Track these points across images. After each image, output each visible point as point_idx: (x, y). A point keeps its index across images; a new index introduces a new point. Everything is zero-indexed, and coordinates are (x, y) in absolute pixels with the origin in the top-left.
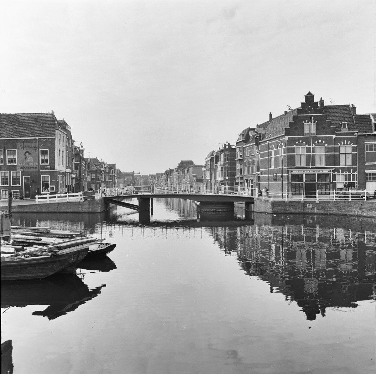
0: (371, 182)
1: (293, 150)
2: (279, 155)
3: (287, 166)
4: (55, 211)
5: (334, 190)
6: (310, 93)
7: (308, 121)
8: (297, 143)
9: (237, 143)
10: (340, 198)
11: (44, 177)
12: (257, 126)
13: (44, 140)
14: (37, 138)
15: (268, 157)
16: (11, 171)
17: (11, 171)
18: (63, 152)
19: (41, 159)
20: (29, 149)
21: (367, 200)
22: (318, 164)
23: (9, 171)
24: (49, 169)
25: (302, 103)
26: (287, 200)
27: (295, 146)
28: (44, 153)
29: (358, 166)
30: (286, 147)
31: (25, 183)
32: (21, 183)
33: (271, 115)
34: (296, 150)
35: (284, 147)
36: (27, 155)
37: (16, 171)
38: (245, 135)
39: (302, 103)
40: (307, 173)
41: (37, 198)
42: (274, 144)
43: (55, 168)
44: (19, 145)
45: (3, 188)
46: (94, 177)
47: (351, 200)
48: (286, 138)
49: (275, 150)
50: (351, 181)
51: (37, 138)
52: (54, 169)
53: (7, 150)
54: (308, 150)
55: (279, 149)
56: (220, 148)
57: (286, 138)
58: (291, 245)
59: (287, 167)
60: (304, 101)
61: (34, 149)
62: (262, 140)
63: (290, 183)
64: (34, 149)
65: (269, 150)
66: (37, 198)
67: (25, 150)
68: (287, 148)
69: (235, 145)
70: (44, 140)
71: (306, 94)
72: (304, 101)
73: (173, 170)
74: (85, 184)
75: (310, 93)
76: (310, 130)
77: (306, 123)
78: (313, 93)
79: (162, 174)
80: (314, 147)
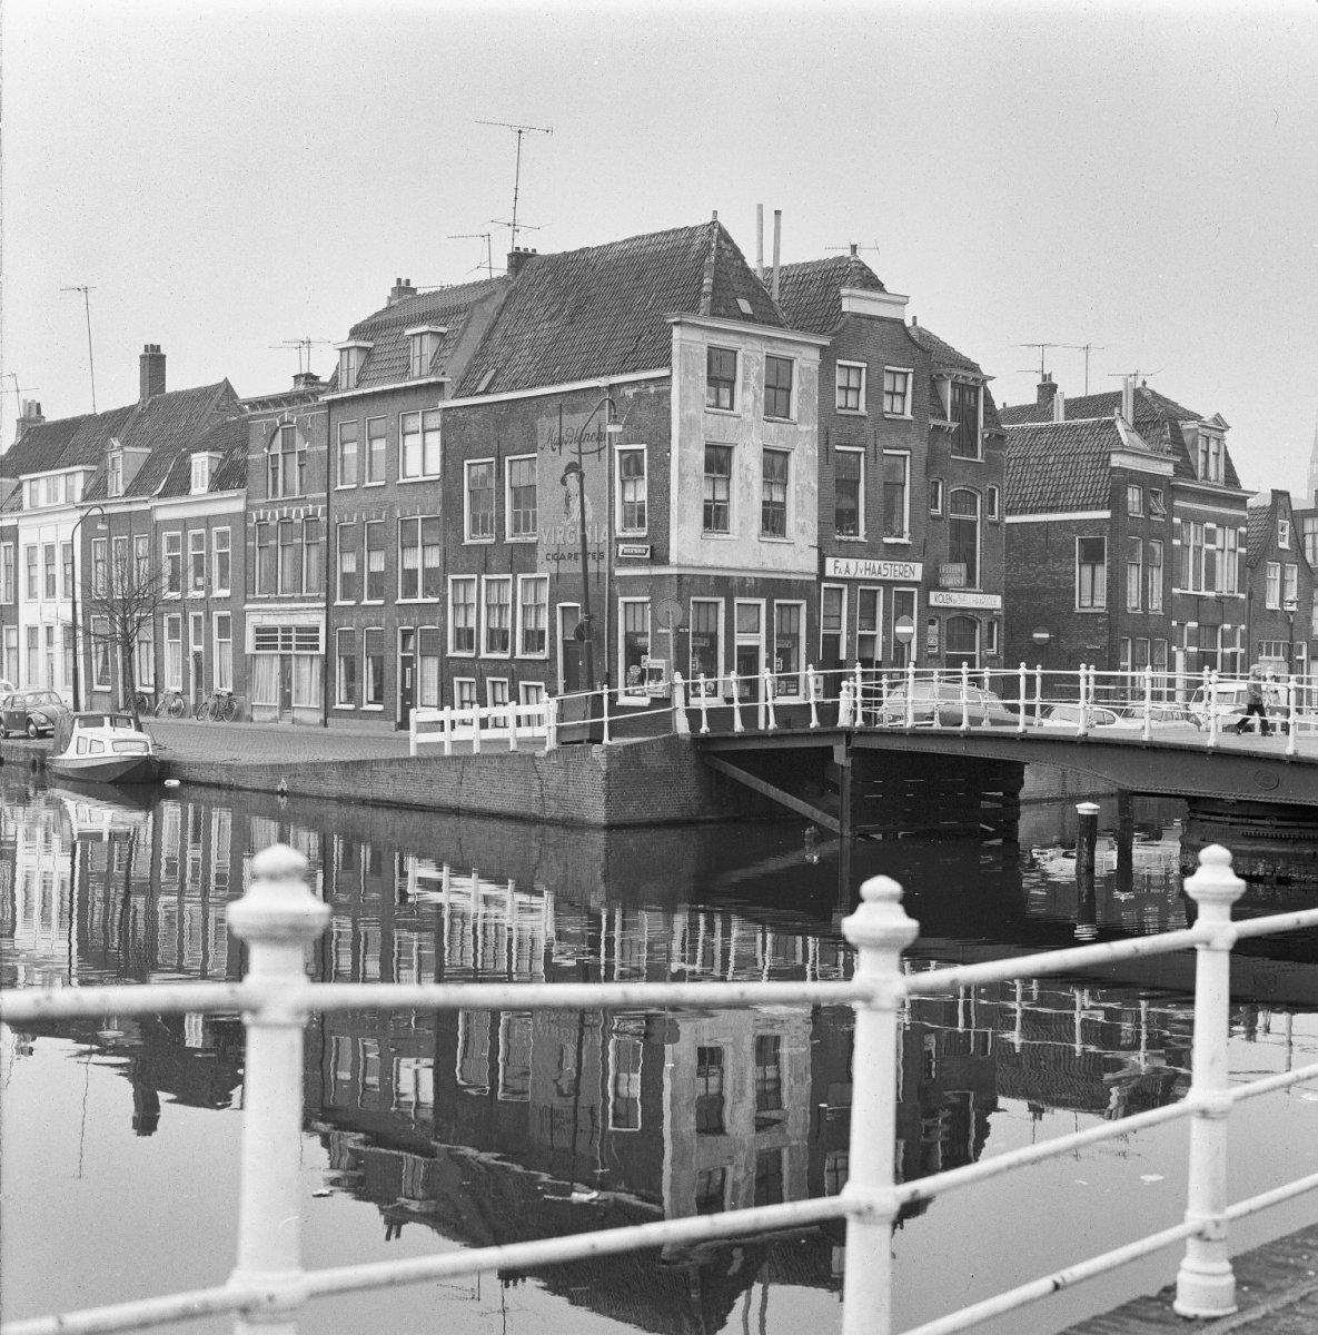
0: (738, 565)
4: (451, 801)
5: (606, 686)
10: (213, 877)
11: (630, 607)
13: (630, 392)
14: (602, 382)
16: (520, 576)
19: (623, 502)
24: (638, 562)
28: (632, 466)
29: (1056, 429)
31: (565, 642)
32: (550, 647)
37: (534, 576)
41: (1031, 672)
43: (673, 558)
44: (546, 425)
45: (491, 667)
46: (1294, 608)
50: (1200, 590)
51: (602, 382)
52: (665, 561)
53: (507, 458)
58: (523, 1201)
66: (1031, 672)
70: (630, 392)
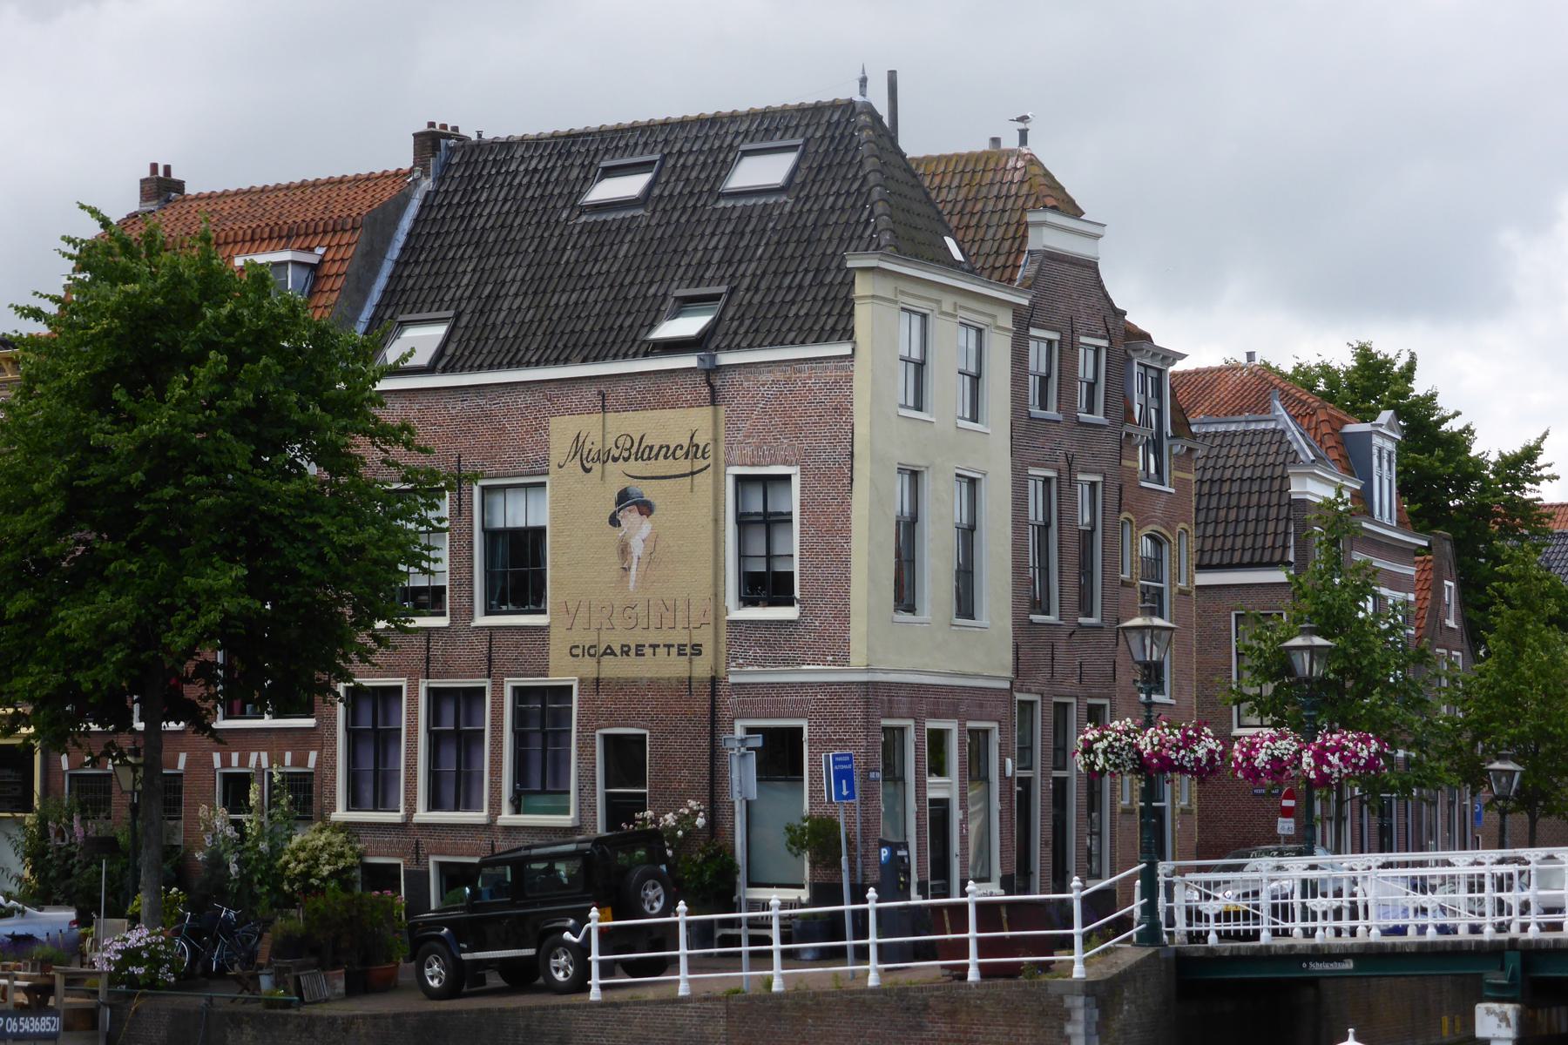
17: (509, 684)
20: (636, 467)
36: (630, 518)
47: (985, 971)
61: (684, 466)
64: (684, 466)
67: (617, 477)
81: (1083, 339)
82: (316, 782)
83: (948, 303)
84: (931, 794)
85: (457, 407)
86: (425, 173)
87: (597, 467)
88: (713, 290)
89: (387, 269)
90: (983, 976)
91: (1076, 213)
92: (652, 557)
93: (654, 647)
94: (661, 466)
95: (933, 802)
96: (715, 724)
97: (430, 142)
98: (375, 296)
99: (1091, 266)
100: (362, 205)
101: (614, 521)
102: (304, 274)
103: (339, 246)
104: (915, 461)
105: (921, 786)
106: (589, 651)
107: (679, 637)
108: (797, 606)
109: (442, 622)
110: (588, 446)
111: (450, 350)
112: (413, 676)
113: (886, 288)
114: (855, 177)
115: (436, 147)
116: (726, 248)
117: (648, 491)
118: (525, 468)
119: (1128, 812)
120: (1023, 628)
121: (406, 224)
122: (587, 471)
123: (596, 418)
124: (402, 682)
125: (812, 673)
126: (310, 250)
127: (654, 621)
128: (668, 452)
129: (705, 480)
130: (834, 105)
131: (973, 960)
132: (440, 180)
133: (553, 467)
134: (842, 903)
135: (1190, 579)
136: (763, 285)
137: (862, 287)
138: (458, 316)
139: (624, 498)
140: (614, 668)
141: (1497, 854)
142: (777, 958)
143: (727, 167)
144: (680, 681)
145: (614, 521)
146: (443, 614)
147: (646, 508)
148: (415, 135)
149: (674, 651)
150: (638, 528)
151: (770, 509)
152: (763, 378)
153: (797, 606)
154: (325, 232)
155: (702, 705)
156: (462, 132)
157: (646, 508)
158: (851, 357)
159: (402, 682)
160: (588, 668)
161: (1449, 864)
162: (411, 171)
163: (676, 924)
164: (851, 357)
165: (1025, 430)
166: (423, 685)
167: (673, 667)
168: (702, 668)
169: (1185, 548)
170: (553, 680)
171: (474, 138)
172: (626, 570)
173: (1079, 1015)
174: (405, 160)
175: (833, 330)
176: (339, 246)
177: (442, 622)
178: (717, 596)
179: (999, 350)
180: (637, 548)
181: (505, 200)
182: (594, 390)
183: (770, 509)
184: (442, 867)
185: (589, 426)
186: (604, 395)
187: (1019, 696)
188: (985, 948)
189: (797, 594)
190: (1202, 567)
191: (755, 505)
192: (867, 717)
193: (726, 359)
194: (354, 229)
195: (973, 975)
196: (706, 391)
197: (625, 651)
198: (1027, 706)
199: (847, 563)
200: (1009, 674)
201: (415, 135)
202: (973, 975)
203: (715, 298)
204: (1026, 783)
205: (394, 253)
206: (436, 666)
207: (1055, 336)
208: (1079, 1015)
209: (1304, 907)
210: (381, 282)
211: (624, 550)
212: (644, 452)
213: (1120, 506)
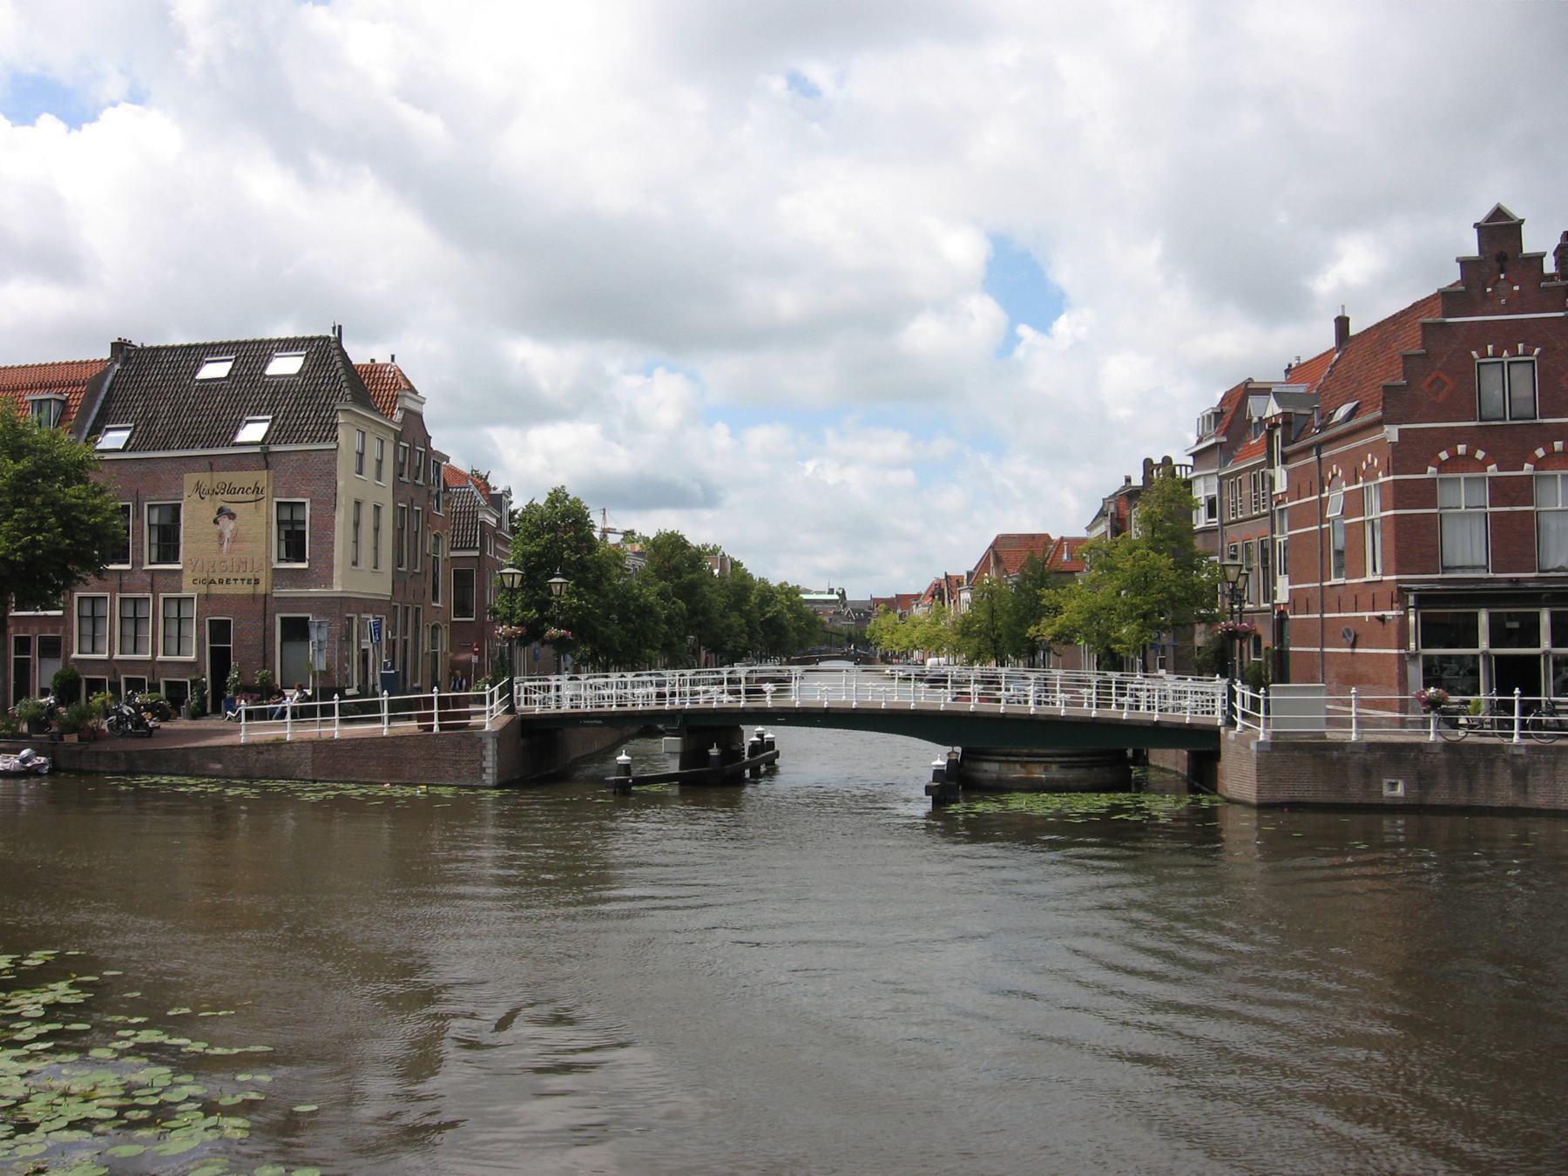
1: (1426, 493)
2: (1361, 519)
3: (1397, 573)
6: (1499, 213)
7: (1494, 351)
8: (1444, 456)
9: (1195, 455)
12: (1287, 371)
15: (1317, 528)
17: (162, 595)
18: (377, 508)
20: (227, 497)
21: (1522, 736)
22: (1232, 571)
23: (151, 596)
25: (1465, 263)
26: (1354, 737)
27: (1528, 468)
30: (1391, 478)
33: (1342, 323)
34: (1445, 495)
35: (1383, 476)
36: (224, 521)
38: (1227, 417)
39: (1465, 263)
40: (13, 653)
42: (1339, 459)
47: (442, 727)
48: (1392, 433)
49: (1345, 493)
54: (1501, 491)
55: (1360, 485)
56: (1128, 480)
57: (1392, 433)
59: (1394, 577)
60: (1472, 249)
61: (252, 497)
62: (1294, 442)
63: (1414, 657)
64: (252, 497)
65: (1322, 491)
67: (219, 501)
68: (1394, 480)
69: (1190, 461)
71: (1481, 214)
72: (1472, 249)
73: (959, 582)
74: (1404, 618)
75: (1499, 213)
76: (1507, 385)
77: (1487, 357)
78: (1517, 212)
79: (919, 596)
80: (1531, 476)
81: (418, 448)
82: (63, 641)
83: (373, 428)
84: (363, 647)
85: (137, 468)
86: (117, 361)
87: (207, 497)
88: (128, 425)
89: (99, 403)
90: (441, 729)
91: (416, 393)
92: (235, 539)
93: (236, 580)
94: (240, 497)
95: (364, 650)
96: (266, 615)
97: (119, 347)
98: (93, 417)
99: (420, 416)
100: (87, 374)
101: (216, 522)
102: (58, 405)
103: (76, 392)
104: (360, 498)
105: (359, 643)
106: (203, 581)
107: (249, 575)
108: (307, 562)
109: (128, 567)
110: (203, 486)
111: (133, 441)
112: (113, 592)
113: (351, 419)
114: (332, 370)
115: (122, 349)
116: (270, 399)
117: (233, 508)
118: (171, 497)
119: (427, 654)
120: (396, 576)
121: (107, 383)
122: (203, 498)
123: (208, 474)
124: (108, 594)
125: (314, 591)
126: (61, 393)
127: (235, 569)
128: (243, 490)
129: (264, 503)
130: (320, 338)
131: (436, 722)
132: (123, 364)
133: (186, 495)
134: (1540, 696)
135: (448, 554)
136: (291, 416)
137: (341, 419)
138: (135, 427)
139: (221, 511)
140: (217, 589)
141: (634, 674)
142: (337, 722)
143: (198, 367)
144: (248, 595)
145: (216, 522)
146: (128, 563)
147: (232, 516)
148: (112, 344)
149: (245, 582)
150: (228, 526)
151: (295, 518)
152: (292, 458)
153: (307, 562)
154: (69, 386)
155: (260, 607)
156: (133, 343)
157: (232, 516)
158: (336, 450)
159: (108, 594)
160: (203, 589)
161: (548, 680)
162: (108, 360)
163: (334, 705)
164: (336, 450)
165: (398, 485)
166: (118, 596)
167: (247, 589)
168: (261, 589)
169: (445, 543)
170: (184, 594)
171: (140, 346)
172: (222, 545)
173: (490, 747)
174: (106, 355)
175: (327, 437)
176: (76, 392)
177: (128, 567)
178: (268, 558)
179: (389, 449)
180: (228, 535)
181: (158, 374)
182: (207, 462)
183: (295, 518)
184: (127, 679)
185: (206, 478)
186: (212, 464)
187: (394, 604)
188: (441, 717)
189: (307, 556)
190: (452, 549)
191: (286, 516)
192: (340, 612)
193: (274, 448)
194: (84, 385)
195: (436, 729)
196: (263, 463)
197: (221, 581)
198: (396, 607)
199: (332, 543)
200: (390, 594)
201: (112, 344)
202: (436, 729)
203: (267, 421)
204: (394, 641)
205: (102, 397)
206: (125, 588)
207: (407, 445)
208: (490, 747)
209: (526, 698)
210: (96, 410)
211: (221, 535)
212: (232, 490)
213: (1299, 492)
